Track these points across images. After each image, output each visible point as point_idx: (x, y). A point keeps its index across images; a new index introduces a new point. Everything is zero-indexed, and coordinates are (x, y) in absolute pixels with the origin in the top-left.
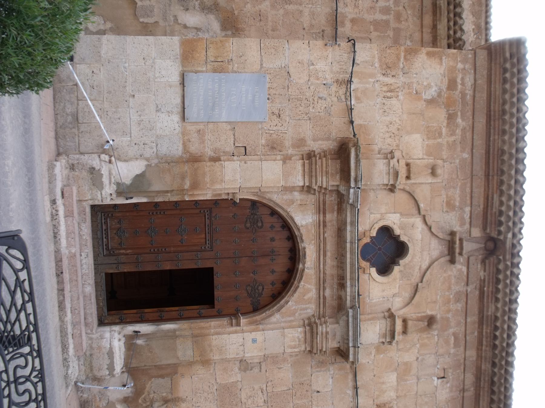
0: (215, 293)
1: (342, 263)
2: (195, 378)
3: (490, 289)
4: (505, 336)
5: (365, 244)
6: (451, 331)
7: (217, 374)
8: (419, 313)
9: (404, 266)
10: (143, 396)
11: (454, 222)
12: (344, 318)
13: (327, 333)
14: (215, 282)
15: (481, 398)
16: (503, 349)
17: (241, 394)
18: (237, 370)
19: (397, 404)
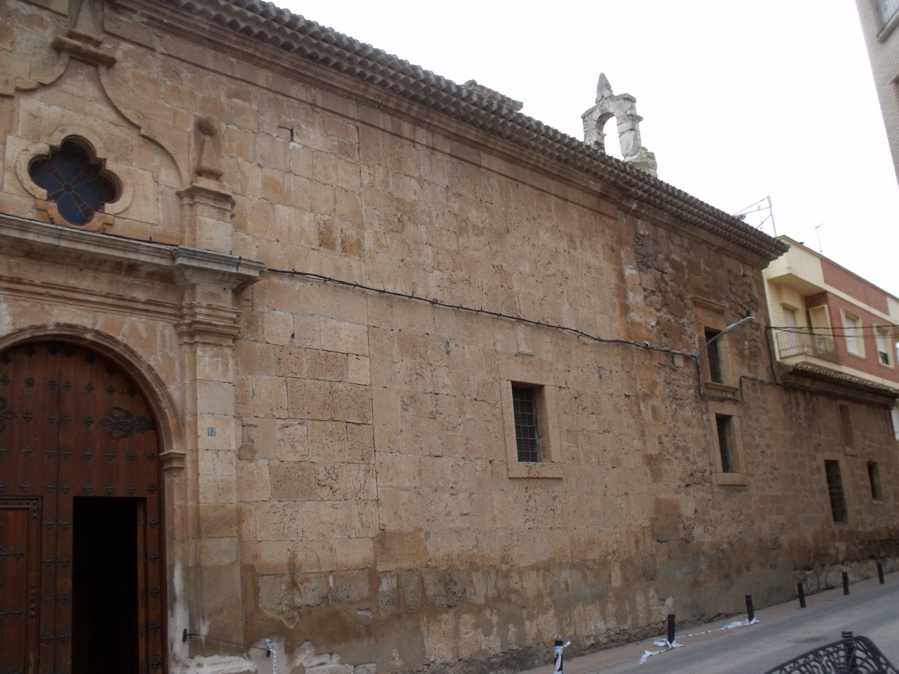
0: (120, 495)
1: (91, 262)
2: (261, 536)
3: (167, 12)
4: (250, 14)
5: (61, 213)
6: (223, 99)
7: (256, 499)
8: (189, 146)
9: (108, 151)
10: (285, 622)
11: (35, 37)
12: (188, 274)
13: (209, 307)
14: (100, 495)
15: (330, 82)
16: (268, 25)
17: (289, 462)
18: (252, 466)
19: (322, 214)
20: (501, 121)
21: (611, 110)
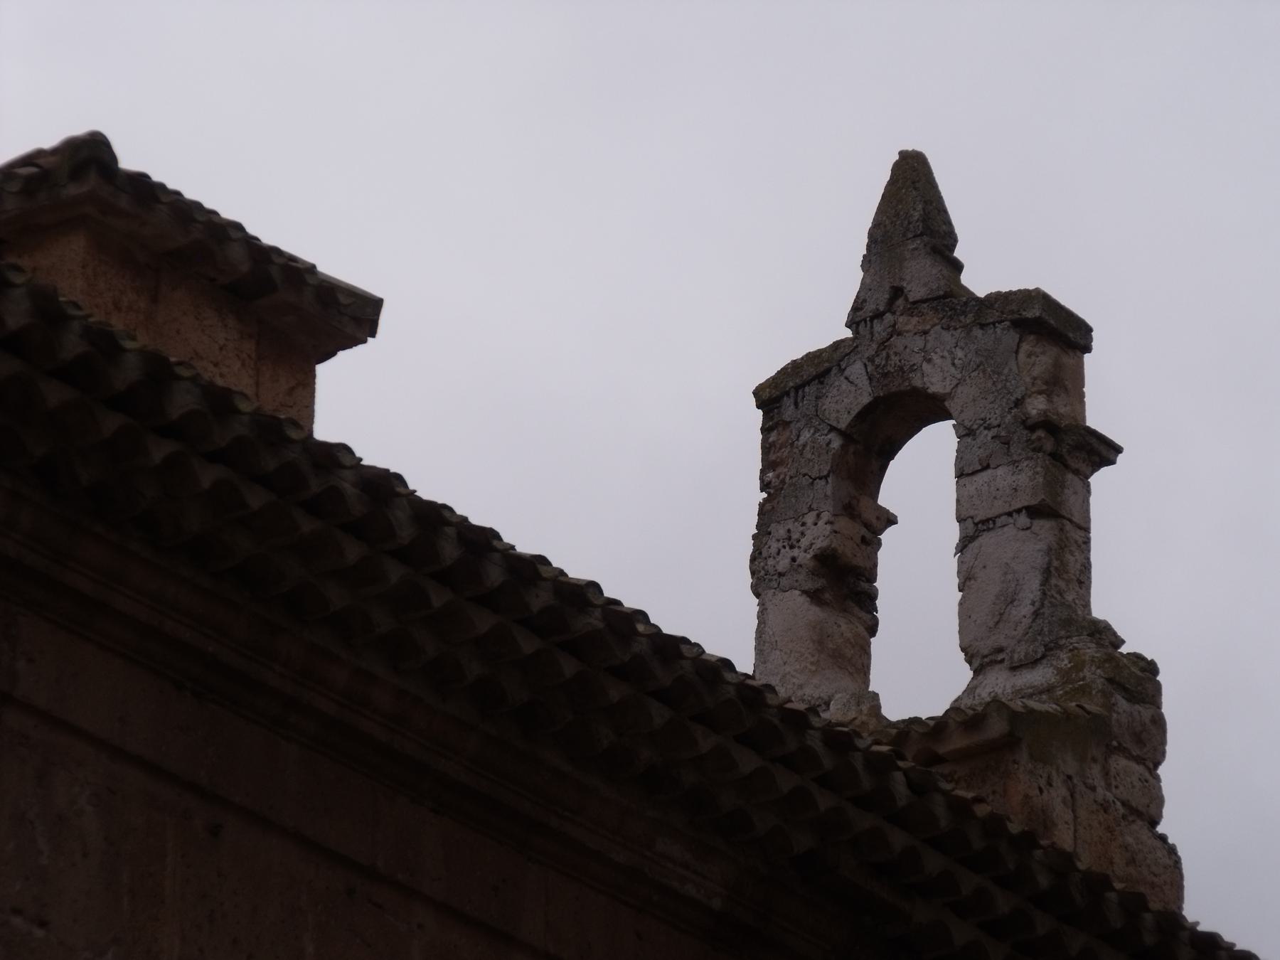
20: (160, 451)
21: (935, 380)
